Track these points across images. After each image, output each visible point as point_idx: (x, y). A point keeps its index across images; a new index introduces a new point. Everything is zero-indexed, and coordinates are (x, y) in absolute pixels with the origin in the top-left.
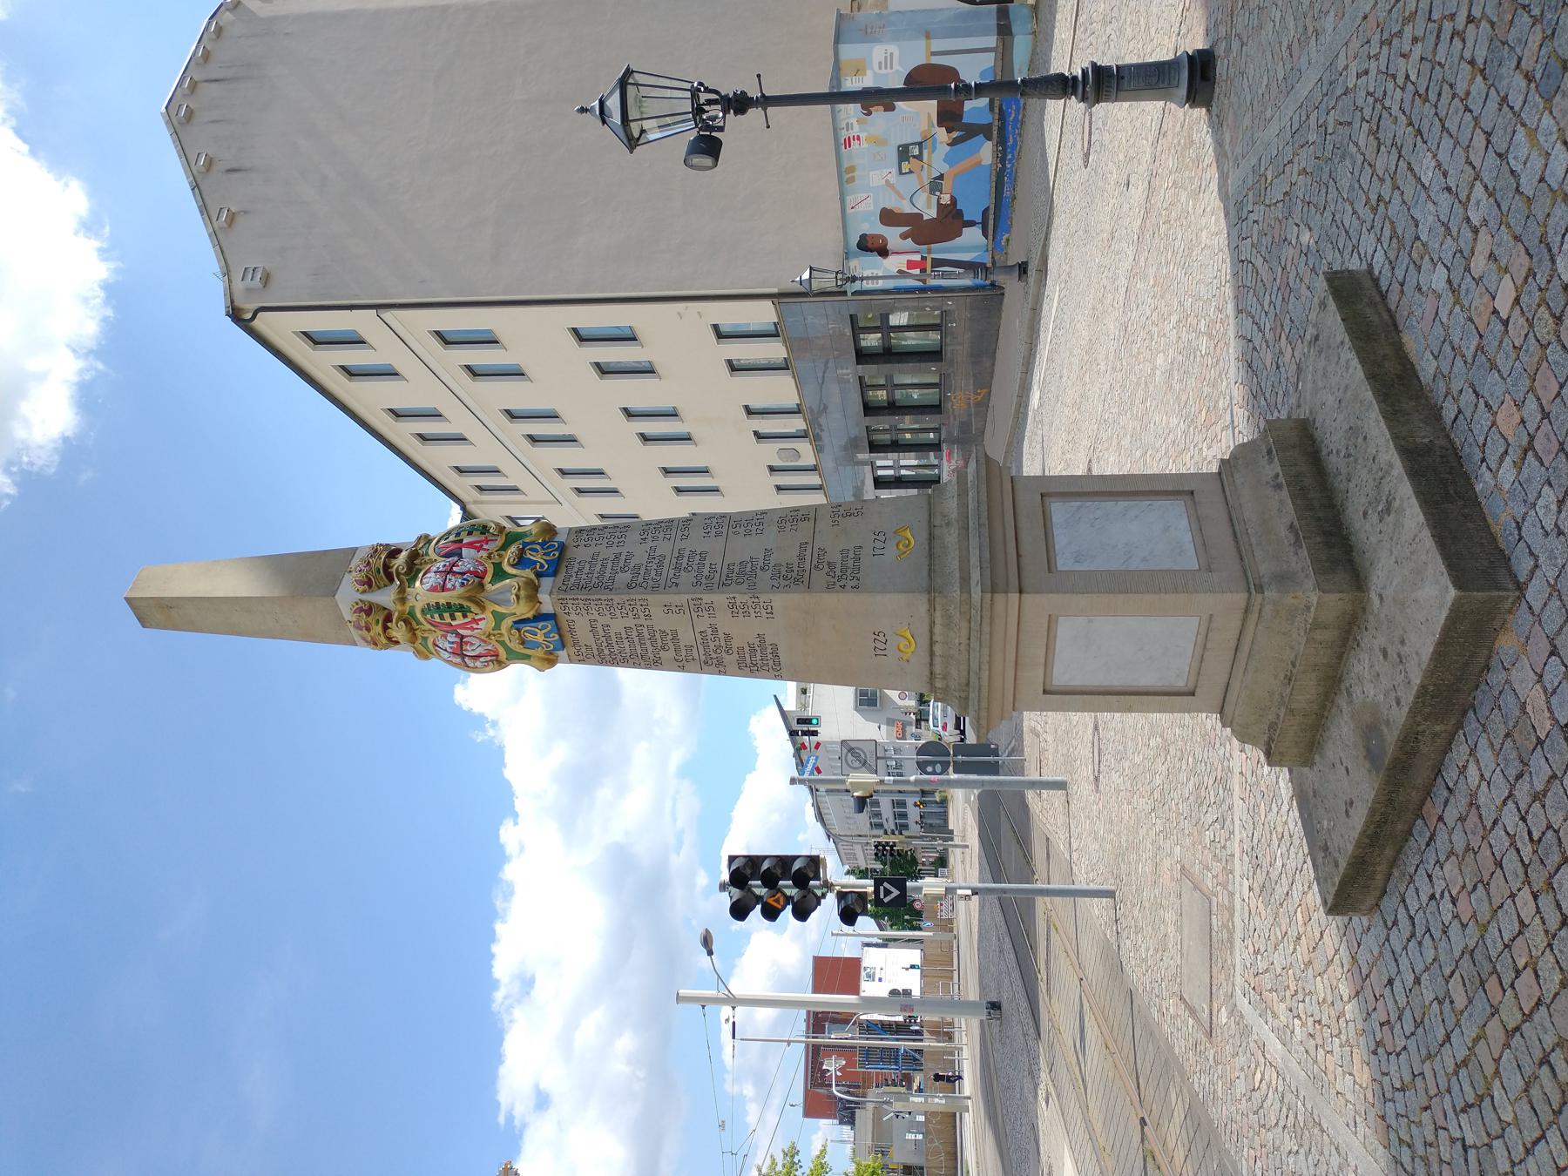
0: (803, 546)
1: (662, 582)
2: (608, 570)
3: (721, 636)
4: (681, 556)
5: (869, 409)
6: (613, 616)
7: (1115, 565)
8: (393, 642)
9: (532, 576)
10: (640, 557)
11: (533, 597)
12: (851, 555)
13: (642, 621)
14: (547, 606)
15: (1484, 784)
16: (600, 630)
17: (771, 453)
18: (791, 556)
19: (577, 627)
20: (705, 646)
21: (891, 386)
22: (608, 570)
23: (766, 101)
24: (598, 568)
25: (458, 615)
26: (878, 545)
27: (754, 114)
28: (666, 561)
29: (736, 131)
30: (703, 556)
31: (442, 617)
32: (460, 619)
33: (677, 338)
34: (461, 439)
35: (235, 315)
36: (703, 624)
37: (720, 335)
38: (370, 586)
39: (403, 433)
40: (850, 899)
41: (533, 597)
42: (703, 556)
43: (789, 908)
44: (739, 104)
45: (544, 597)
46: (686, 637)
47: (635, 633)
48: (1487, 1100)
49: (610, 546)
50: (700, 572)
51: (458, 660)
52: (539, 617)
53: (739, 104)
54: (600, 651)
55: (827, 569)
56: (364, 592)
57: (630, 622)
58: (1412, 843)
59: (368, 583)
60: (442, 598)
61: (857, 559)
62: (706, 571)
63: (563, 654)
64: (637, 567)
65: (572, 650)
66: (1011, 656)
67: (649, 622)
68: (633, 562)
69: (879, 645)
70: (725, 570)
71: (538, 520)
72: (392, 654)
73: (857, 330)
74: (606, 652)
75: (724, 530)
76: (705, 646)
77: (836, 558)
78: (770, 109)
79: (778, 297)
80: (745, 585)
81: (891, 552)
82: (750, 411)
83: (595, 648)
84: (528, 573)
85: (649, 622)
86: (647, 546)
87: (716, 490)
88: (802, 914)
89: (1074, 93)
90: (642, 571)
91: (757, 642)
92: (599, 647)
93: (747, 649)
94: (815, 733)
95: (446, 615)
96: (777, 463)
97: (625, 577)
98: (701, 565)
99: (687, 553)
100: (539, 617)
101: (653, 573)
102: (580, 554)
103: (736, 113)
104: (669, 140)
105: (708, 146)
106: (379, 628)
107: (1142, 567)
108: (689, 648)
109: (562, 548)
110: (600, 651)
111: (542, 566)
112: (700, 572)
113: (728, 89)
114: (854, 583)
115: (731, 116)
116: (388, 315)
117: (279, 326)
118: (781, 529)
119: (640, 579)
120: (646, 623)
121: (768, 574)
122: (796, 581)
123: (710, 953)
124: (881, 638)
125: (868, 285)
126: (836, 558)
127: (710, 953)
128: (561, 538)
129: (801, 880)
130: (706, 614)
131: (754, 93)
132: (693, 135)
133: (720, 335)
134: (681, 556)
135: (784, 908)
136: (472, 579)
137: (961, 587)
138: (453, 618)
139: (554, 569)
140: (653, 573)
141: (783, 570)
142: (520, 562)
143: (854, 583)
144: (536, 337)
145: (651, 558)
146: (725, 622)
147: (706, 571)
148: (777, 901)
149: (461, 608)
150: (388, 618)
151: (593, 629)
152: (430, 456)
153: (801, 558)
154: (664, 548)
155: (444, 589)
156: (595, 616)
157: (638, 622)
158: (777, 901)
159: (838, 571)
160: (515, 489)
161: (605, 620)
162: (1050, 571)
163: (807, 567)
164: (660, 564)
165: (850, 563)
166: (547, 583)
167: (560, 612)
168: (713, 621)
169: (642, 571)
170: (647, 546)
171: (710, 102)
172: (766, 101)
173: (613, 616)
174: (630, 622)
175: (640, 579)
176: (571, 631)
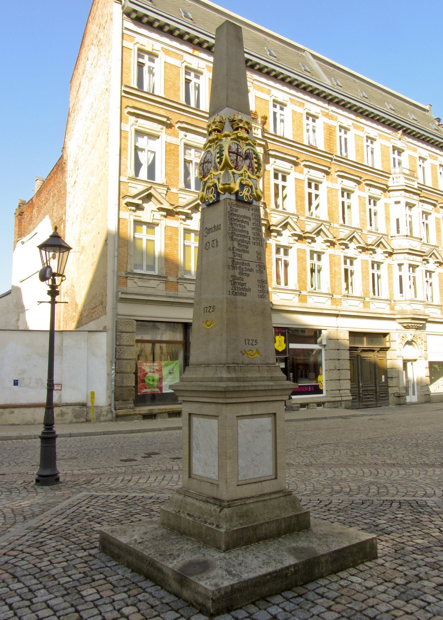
3: (248, 272)
11: (225, 190)
14: (222, 198)
15: (423, 604)
26: (250, 342)
41: (225, 190)
45: (227, 195)
48: (96, 602)
52: (218, 194)
58: (142, 577)
59: (232, 121)
71: (263, 193)
84: (237, 188)
89: (46, 429)
91: (247, 287)
95: (218, 155)
100: (218, 194)
103: (48, 291)
106: (214, 127)
109: (250, 203)
111: (241, 194)
124: (254, 343)
128: (255, 203)
131: (57, 298)
137: (230, 378)
149: (221, 161)
150: (219, 131)
155: (229, 152)
166: (233, 197)
172: (53, 303)
174: (251, 235)
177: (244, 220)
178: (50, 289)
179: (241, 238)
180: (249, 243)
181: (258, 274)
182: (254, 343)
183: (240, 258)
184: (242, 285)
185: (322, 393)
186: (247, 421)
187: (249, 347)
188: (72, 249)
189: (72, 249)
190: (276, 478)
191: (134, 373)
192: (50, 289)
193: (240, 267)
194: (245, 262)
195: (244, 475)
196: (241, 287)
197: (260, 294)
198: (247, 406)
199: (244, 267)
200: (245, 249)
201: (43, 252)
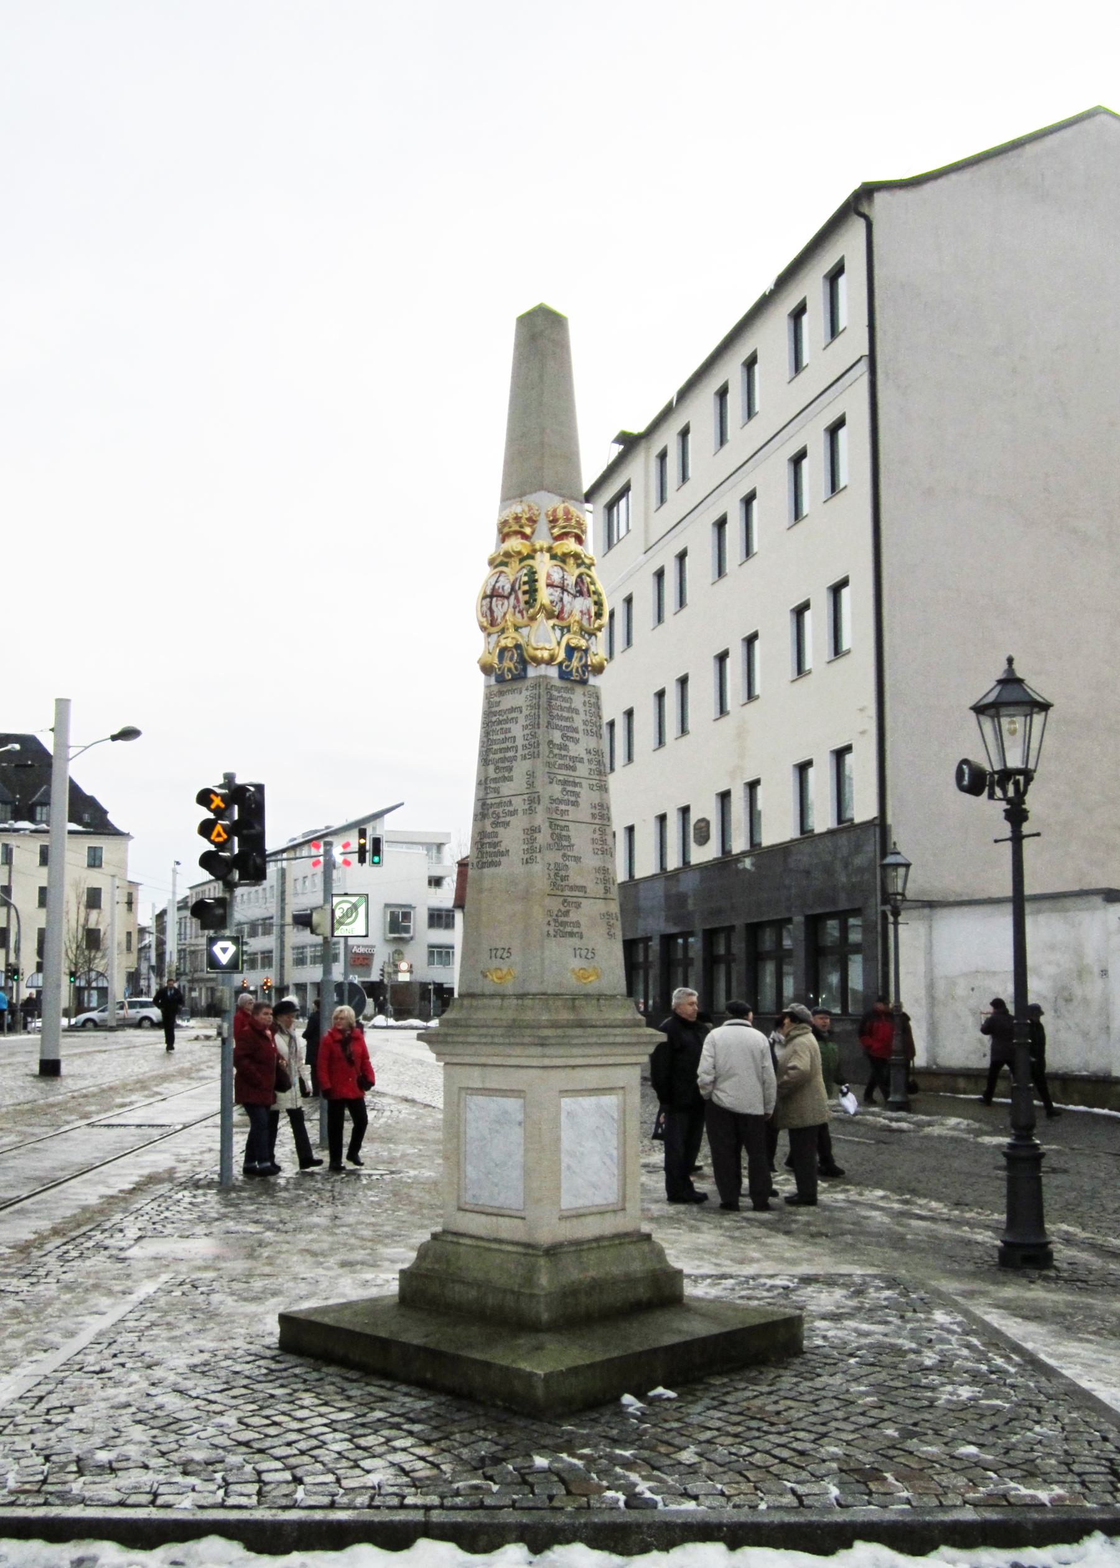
0: (582, 888)
1: (555, 816)
2: (564, 723)
3: (508, 819)
4: (575, 784)
5: (754, 930)
6: (525, 727)
7: (565, 1144)
8: (504, 537)
9: (559, 659)
10: (575, 750)
12: (575, 930)
13: (520, 752)
16: (514, 715)
17: (706, 809)
18: (575, 879)
19: (516, 695)
20: (500, 804)
21: (781, 957)
22: (564, 723)
23: (1017, 839)
24: (565, 714)
25: (527, 597)
26: (584, 952)
27: (1006, 829)
28: (572, 773)
29: (990, 810)
30: (575, 804)
31: (525, 583)
32: (523, 598)
33: (832, 706)
34: (723, 440)
35: (867, 192)
36: (519, 803)
37: (840, 754)
38: (551, 522)
39: (731, 371)
40: (219, 911)
42: (575, 804)
43: (212, 848)
44: (1016, 814)
46: (507, 789)
47: (510, 745)
49: (585, 723)
50: (561, 802)
51: (488, 592)
53: (1016, 814)
54: (494, 714)
55: (563, 909)
56: (547, 515)
57: (520, 742)
60: (541, 584)
61: (571, 934)
62: (563, 807)
63: (493, 681)
64: (564, 747)
65: (495, 689)
66: (490, 1061)
67: (519, 758)
68: (571, 745)
69: (499, 953)
70: (563, 823)
72: (493, 534)
73: (842, 916)
74: (494, 719)
75: (597, 821)
76: (500, 804)
77: (573, 917)
78: (1009, 844)
79: (881, 824)
80: (551, 842)
81: (576, 963)
82: (753, 786)
83: (497, 709)
84: (561, 656)
85: (519, 758)
86: (583, 754)
87: (721, 572)
88: (207, 861)
90: (563, 753)
91: (502, 849)
92: (500, 713)
93: (496, 840)
94: (362, 860)
95: (526, 587)
96: (694, 817)
97: (557, 737)
98: (568, 803)
99: (577, 789)
101: (561, 762)
102: (578, 698)
103: (1005, 811)
104: (975, 744)
105: (975, 781)
107: (564, 1166)
108: (496, 790)
109: (584, 682)
110: (494, 714)
112: (561, 802)
113: (1031, 802)
114: (552, 933)
115: (1004, 805)
116: (863, 367)
117: (850, 245)
118: (598, 870)
119: (556, 751)
120: (518, 754)
121: (560, 860)
122: (554, 884)
123: (114, 738)
124: (590, 955)
125: (891, 927)
126: (573, 917)
127: (114, 738)
129: (238, 862)
130: (527, 807)
131: (1026, 828)
132: (988, 768)
133: (840, 754)
134: (575, 784)
135: (212, 842)
136: (557, 609)
138: (525, 593)
139: (564, 675)
140: (561, 762)
141: (563, 873)
142: (570, 650)
143: (552, 933)
144: (837, 536)
145: (574, 759)
146: (519, 823)
147: (563, 807)
148: (219, 835)
151: (513, 710)
152: (704, 401)
153: (572, 888)
154: (583, 770)
156: (525, 712)
157: (520, 748)
158: (219, 835)
159: (561, 919)
160: (662, 500)
161: (522, 721)
162: (561, 1091)
163: (567, 893)
164: (568, 767)
165: (568, 929)
167: (528, 683)
168: (520, 813)
169: (563, 753)
170: (583, 754)
171: (1017, 783)
172: (1017, 839)
173: (525, 727)
174: (520, 742)
175: (556, 751)
176: (513, 691)
177: (510, 716)
178: (1008, 807)
179: (502, 755)
180: (515, 758)
181: (526, 818)
182: (505, 955)
183: (496, 795)
184: (495, 845)
185: (830, 1098)
186: (480, 1100)
187: (496, 963)
188: (1052, 705)
189: (1052, 705)
190: (460, 1209)
191: (503, 999)
192: (1008, 807)
193: (494, 813)
194: (504, 799)
195: (474, 1196)
196: (492, 850)
197: (525, 857)
198: (476, 1072)
199: (500, 810)
200: (506, 774)
201: (988, 725)
